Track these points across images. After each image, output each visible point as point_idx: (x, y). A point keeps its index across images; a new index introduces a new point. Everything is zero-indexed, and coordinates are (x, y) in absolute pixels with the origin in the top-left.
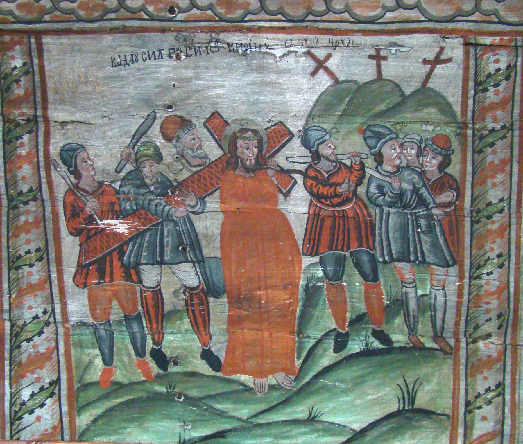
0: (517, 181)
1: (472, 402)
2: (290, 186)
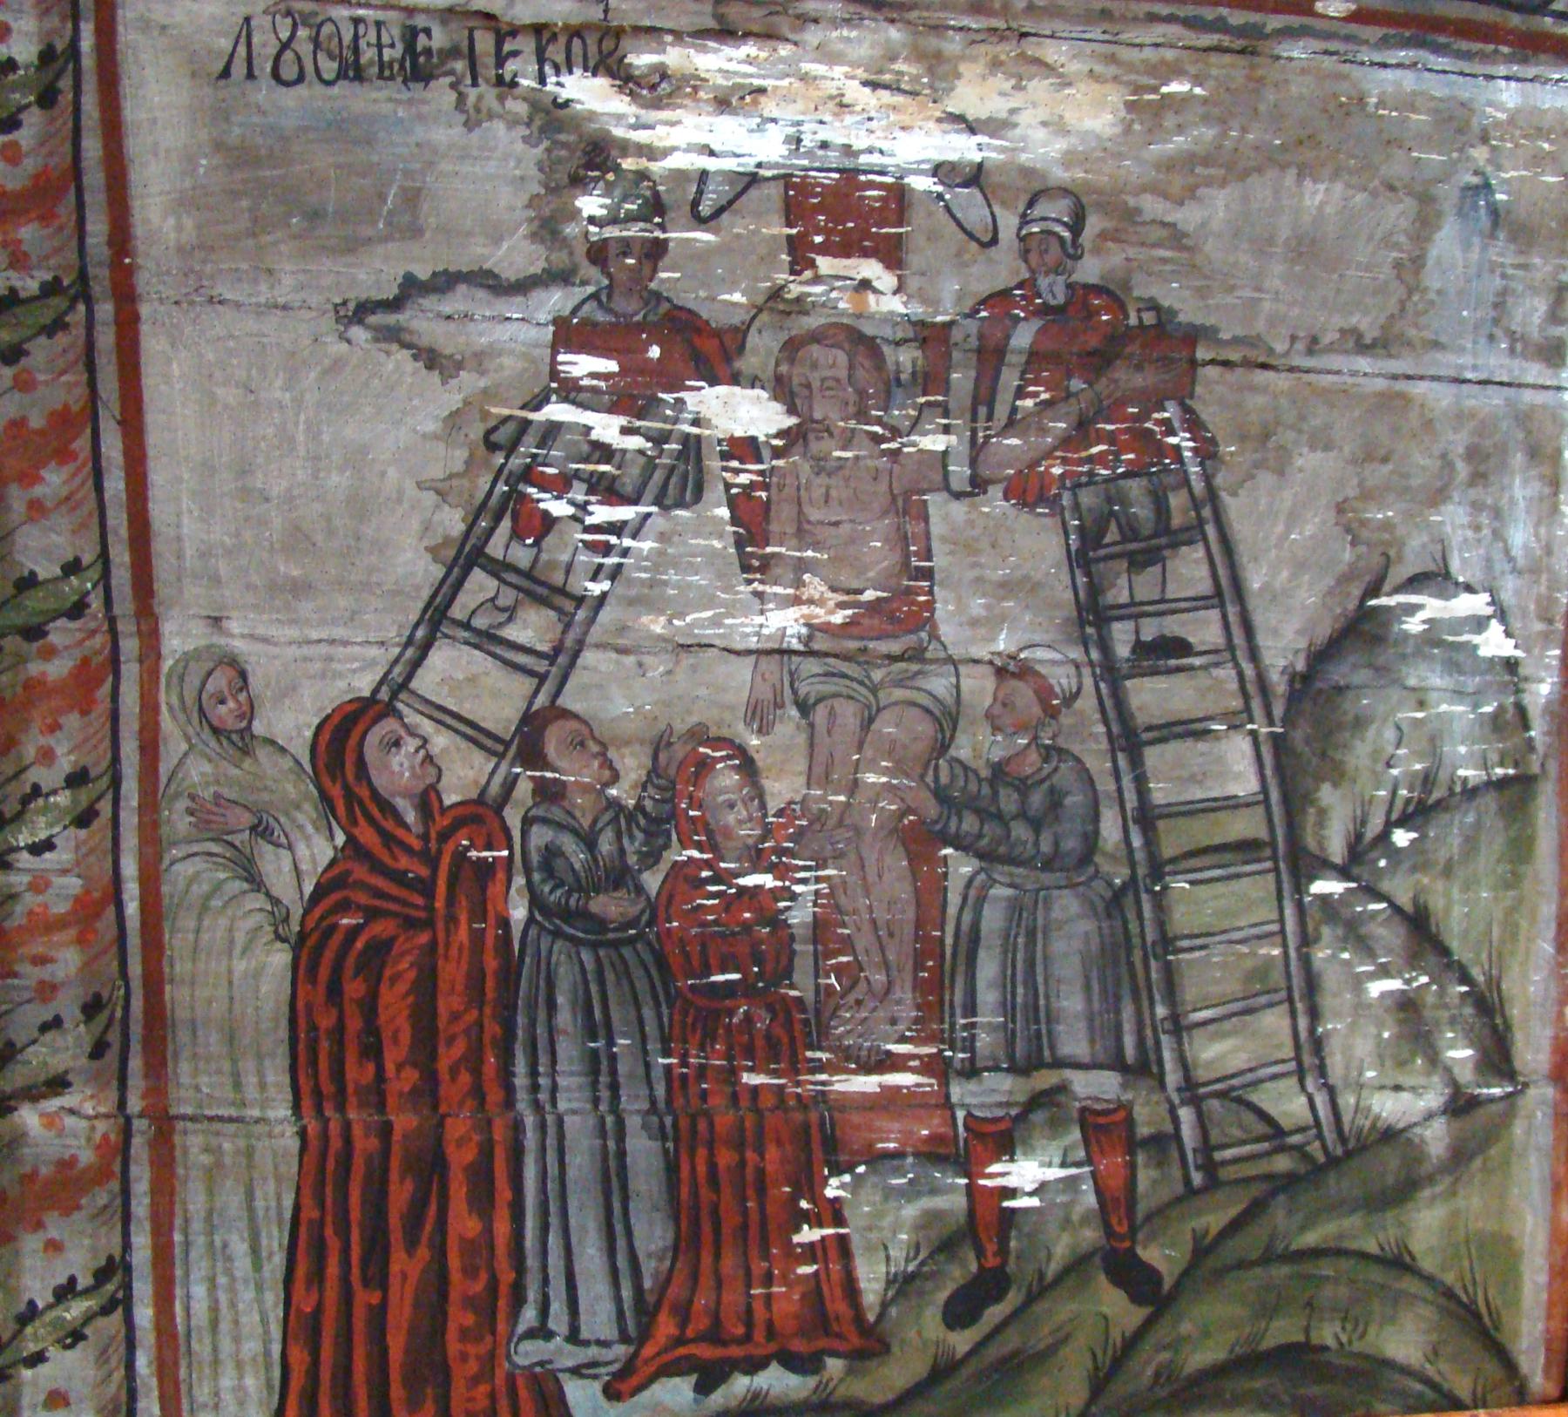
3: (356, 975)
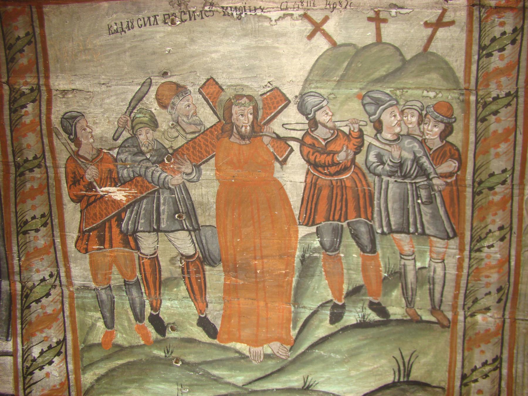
0: (521, 151)
1: (468, 375)
2: (287, 153)
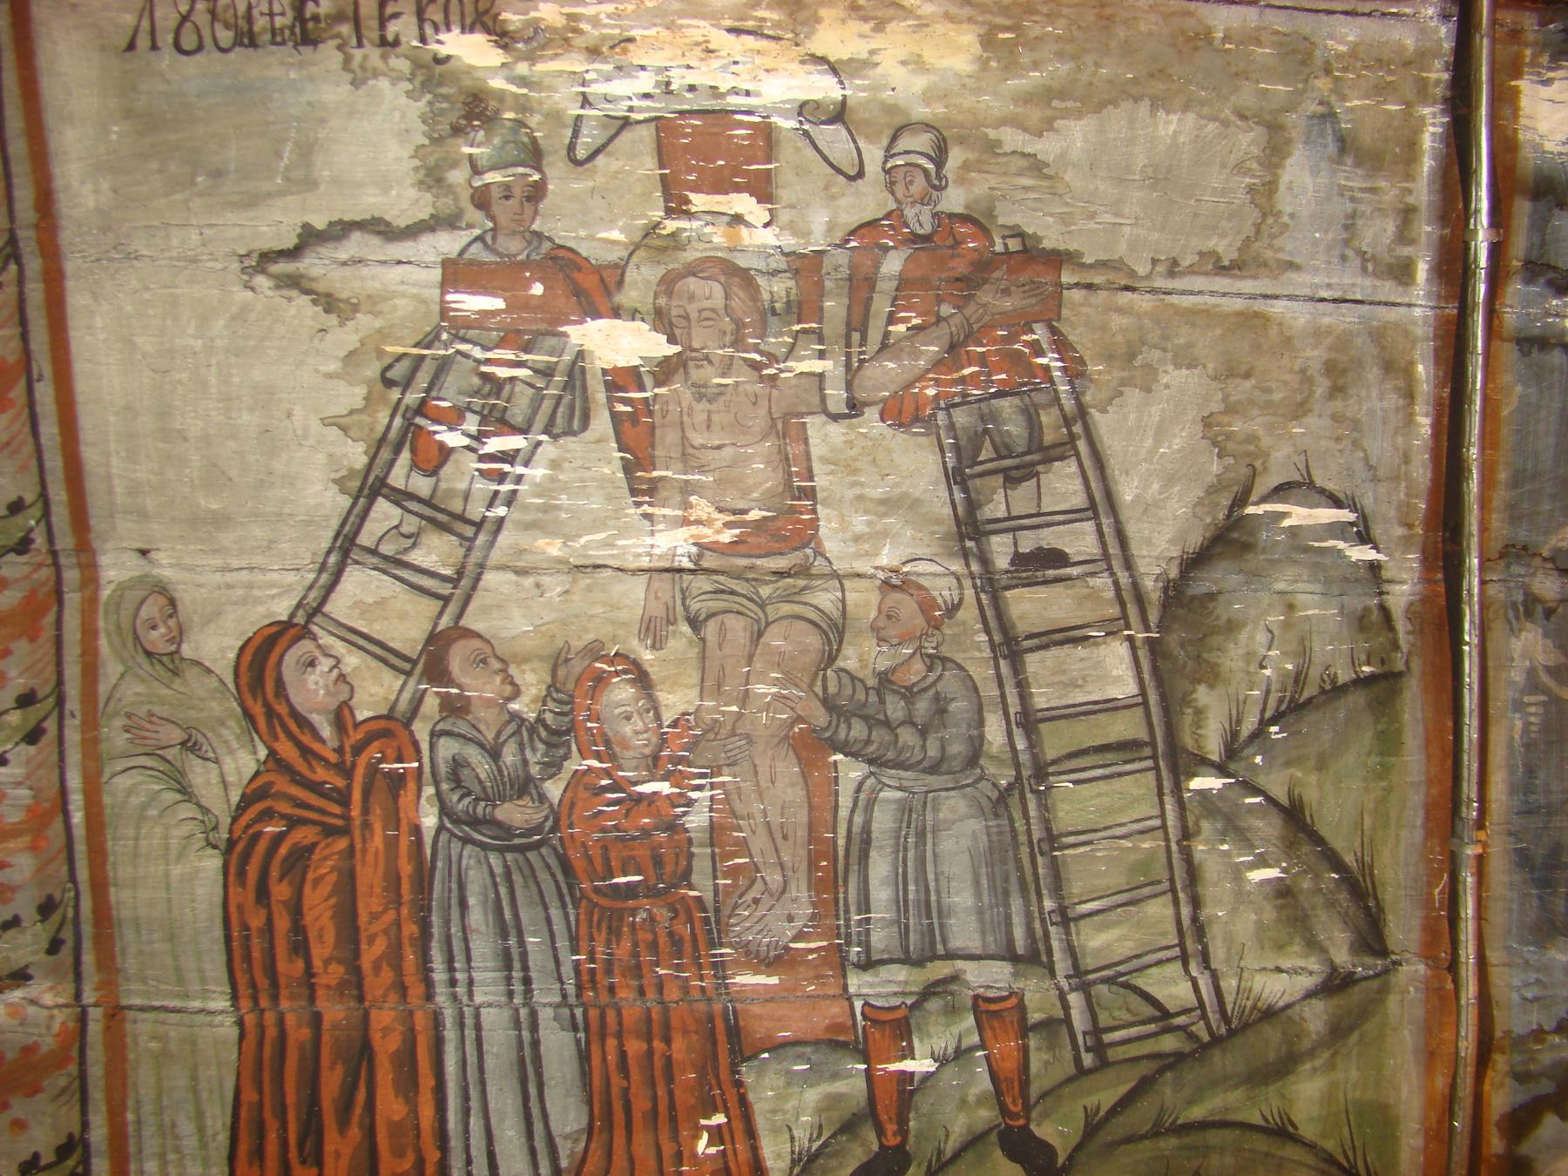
0: (58, 439)
3: (281, 880)
